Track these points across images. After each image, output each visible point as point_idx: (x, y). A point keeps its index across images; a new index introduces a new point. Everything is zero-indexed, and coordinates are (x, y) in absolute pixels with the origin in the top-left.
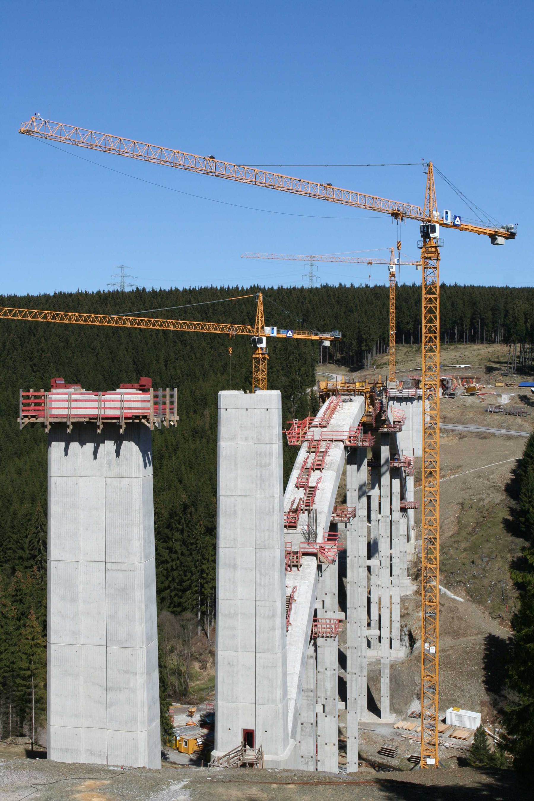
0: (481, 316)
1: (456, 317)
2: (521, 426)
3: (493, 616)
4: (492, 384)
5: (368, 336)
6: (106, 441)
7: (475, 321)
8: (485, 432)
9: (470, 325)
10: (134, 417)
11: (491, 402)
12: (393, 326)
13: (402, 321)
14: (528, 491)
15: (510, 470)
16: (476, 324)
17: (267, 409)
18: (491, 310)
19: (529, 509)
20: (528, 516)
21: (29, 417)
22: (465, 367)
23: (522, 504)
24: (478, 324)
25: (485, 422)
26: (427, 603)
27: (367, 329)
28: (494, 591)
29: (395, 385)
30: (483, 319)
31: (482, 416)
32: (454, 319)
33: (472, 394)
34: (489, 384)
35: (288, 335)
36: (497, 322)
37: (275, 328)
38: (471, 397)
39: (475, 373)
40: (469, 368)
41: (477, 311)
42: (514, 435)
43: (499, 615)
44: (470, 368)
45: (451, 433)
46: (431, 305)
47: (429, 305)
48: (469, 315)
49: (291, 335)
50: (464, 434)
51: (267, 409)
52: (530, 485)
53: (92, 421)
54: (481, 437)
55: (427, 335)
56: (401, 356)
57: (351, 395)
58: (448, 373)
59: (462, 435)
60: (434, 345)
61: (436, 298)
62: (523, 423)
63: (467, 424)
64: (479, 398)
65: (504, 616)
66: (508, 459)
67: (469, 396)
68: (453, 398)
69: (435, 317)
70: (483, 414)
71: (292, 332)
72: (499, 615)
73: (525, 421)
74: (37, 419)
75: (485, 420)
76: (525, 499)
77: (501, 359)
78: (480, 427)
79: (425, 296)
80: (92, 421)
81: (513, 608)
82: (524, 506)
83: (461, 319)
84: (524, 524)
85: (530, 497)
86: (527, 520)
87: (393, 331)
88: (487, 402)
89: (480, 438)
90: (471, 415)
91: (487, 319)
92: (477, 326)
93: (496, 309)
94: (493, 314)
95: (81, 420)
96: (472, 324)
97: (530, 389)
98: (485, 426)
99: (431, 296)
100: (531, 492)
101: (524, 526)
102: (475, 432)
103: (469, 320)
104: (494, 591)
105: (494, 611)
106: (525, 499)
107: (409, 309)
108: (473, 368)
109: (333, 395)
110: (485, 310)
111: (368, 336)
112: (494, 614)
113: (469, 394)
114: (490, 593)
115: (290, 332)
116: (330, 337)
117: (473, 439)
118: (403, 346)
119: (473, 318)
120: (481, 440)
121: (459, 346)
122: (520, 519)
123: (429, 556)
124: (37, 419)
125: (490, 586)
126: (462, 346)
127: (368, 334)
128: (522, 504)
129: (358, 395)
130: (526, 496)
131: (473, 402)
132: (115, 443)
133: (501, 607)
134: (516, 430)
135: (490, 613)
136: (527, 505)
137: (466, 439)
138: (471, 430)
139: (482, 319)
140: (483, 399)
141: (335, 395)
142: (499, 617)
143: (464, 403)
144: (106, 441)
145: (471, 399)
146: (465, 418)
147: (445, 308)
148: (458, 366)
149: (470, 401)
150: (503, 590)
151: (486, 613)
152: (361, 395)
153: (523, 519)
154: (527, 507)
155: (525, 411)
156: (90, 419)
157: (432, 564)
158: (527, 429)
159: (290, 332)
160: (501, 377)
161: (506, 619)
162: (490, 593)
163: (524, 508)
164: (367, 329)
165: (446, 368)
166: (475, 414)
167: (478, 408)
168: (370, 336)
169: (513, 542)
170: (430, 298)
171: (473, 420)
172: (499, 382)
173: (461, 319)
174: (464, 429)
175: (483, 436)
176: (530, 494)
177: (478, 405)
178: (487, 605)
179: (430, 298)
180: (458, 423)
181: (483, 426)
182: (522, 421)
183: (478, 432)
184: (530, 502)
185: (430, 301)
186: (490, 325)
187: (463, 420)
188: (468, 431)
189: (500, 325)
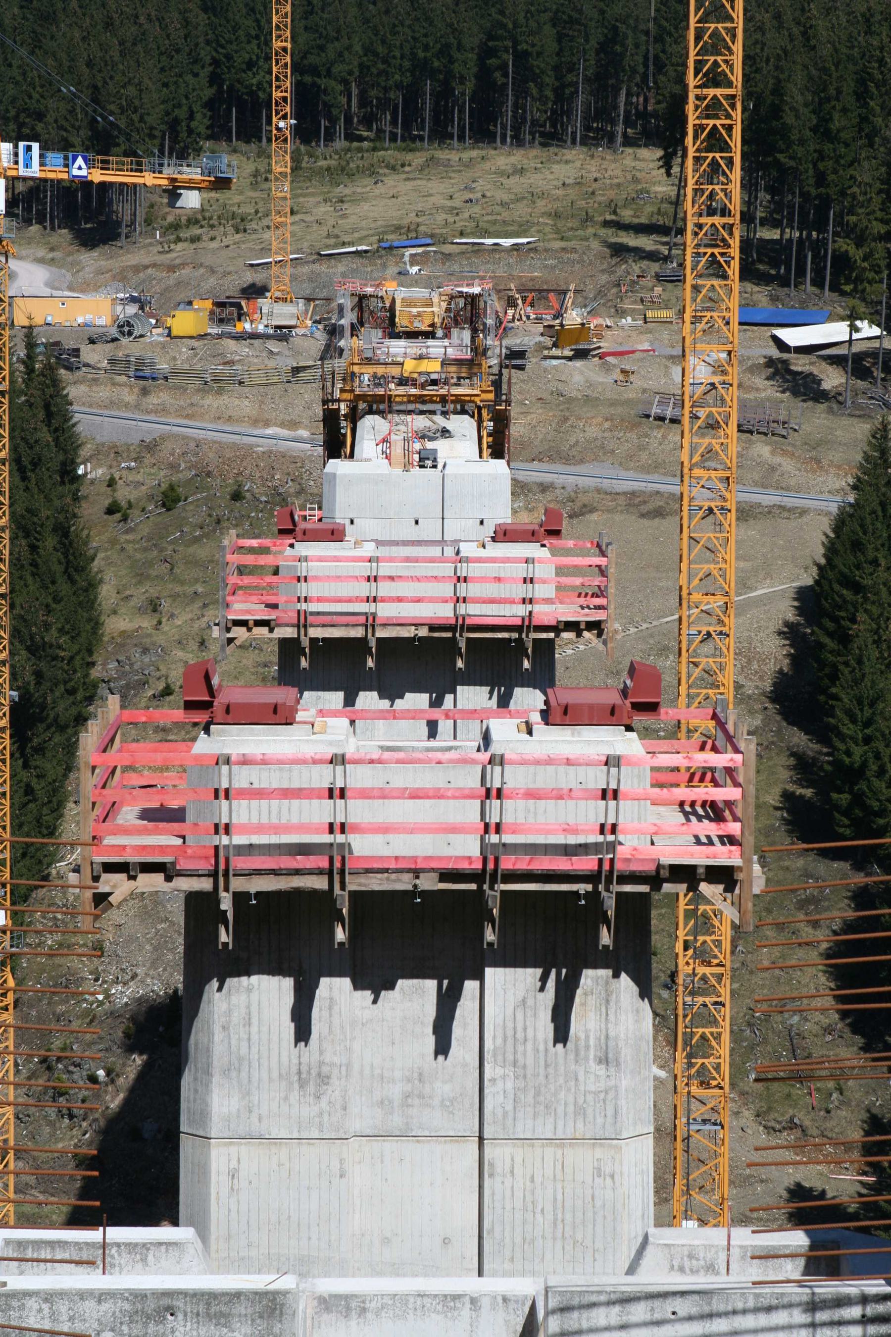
0: (516, 43)
1: (426, 48)
2: (773, 469)
3: (772, 1124)
4: (632, 312)
5: (136, 118)
6: (459, 688)
7: (493, 62)
8: (658, 492)
9: (476, 77)
10: (561, 626)
11: (651, 384)
12: (285, 99)
13: (228, 57)
14: (860, 702)
15: (778, 625)
16: (497, 75)
17: (482, 523)
18: (554, 22)
19: (864, 765)
20: (863, 786)
21: (251, 623)
22: (516, 247)
23: (842, 747)
24: (506, 75)
25: (644, 456)
26: (695, 1090)
27: (131, 91)
28: (765, 1041)
29: (292, 316)
30: (526, 54)
31: (632, 436)
32: (421, 54)
33: (581, 354)
34: (621, 313)
35: (76, 172)
36: (572, 68)
37: (36, 146)
38: (578, 364)
39: (553, 268)
40: (531, 249)
41: (503, 26)
42: (759, 505)
43: (791, 1120)
44: (535, 250)
45: (539, 496)
46: (718, 122)
47: (711, 122)
48: (473, 39)
49: (84, 173)
50: (584, 499)
51: (482, 523)
52: (867, 681)
53: (436, 635)
54: (644, 509)
55: (703, 220)
56: (241, 193)
57: (433, 412)
58: (456, 267)
59: (579, 504)
60: (722, 254)
61: (733, 97)
62: (778, 459)
63: (582, 461)
64: (608, 368)
65: (807, 1123)
66: (752, 589)
67: (570, 359)
68: (521, 368)
69: (730, 162)
70: (633, 426)
71: (85, 160)
72: (791, 1120)
73: (785, 453)
74: (271, 630)
75: (641, 448)
76: (849, 729)
77: (627, 215)
78: (631, 474)
79: (698, 91)
80: (436, 635)
81: (835, 1096)
82: (848, 753)
83: (444, 51)
84: (846, 813)
85: (868, 723)
86: (858, 799)
87: (284, 117)
88: (637, 382)
89: (643, 516)
90: (593, 432)
91: (539, 54)
92: (500, 80)
93: (572, 21)
94: (560, 38)
95: (407, 633)
96: (484, 75)
97: (767, 332)
98: (646, 469)
99: (718, 92)
100: (872, 705)
101: (846, 821)
102: (625, 493)
103: (472, 56)
104: (765, 1041)
105: (770, 1109)
106: (849, 729)
107: (253, 10)
108: (546, 250)
109: (370, 412)
110: (533, 24)
111: (136, 118)
112: (773, 1115)
113: (568, 353)
114: (752, 1047)
115: (80, 161)
116: (199, 177)
117: (618, 517)
118: (235, 151)
119: (486, 53)
120: (646, 522)
121: (442, 155)
122: (834, 796)
123: (701, 938)
124: (271, 630)
125: (750, 1025)
126: (451, 155)
127: (135, 111)
128: (842, 747)
129: (456, 413)
130: (854, 721)
131: (590, 385)
132: (491, 693)
133: (794, 1092)
134: (756, 484)
135: (758, 1116)
136: (858, 751)
137: (594, 517)
138: (606, 484)
139: (521, 57)
140: (623, 371)
141: (380, 413)
142: (792, 1125)
143: (561, 386)
144: (459, 688)
145: (582, 373)
146: (572, 440)
147: (387, 12)
148: (489, 241)
149: (578, 378)
150: (793, 1039)
151: (746, 1113)
152: (463, 412)
153: (843, 799)
154: (857, 758)
155: (781, 418)
156: (432, 628)
157: (709, 964)
158: (792, 482)
159: (80, 161)
160: (658, 290)
161: (815, 1132)
162: (752, 1047)
163: (847, 760)
164: (131, 91)
165: (448, 249)
166: (607, 425)
167: (613, 403)
168: (141, 120)
169: (808, 875)
170: (715, 97)
171: (602, 447)
172: (653, 304)
173: (444, 51)
174: (583, 482)
175: (650, 506)
176: (868, 712)
177: (608, 395)
178: (746, 1089)
179: (715, 97)
180: (551, 459)
181: (635, 469)
182: (773, 453)
183: (633, 494)
184: (867, 740)
185: (713, 108)
186: (549, 79)
187: (565, 448)
188: (598, 490)
189: (587, 79)
